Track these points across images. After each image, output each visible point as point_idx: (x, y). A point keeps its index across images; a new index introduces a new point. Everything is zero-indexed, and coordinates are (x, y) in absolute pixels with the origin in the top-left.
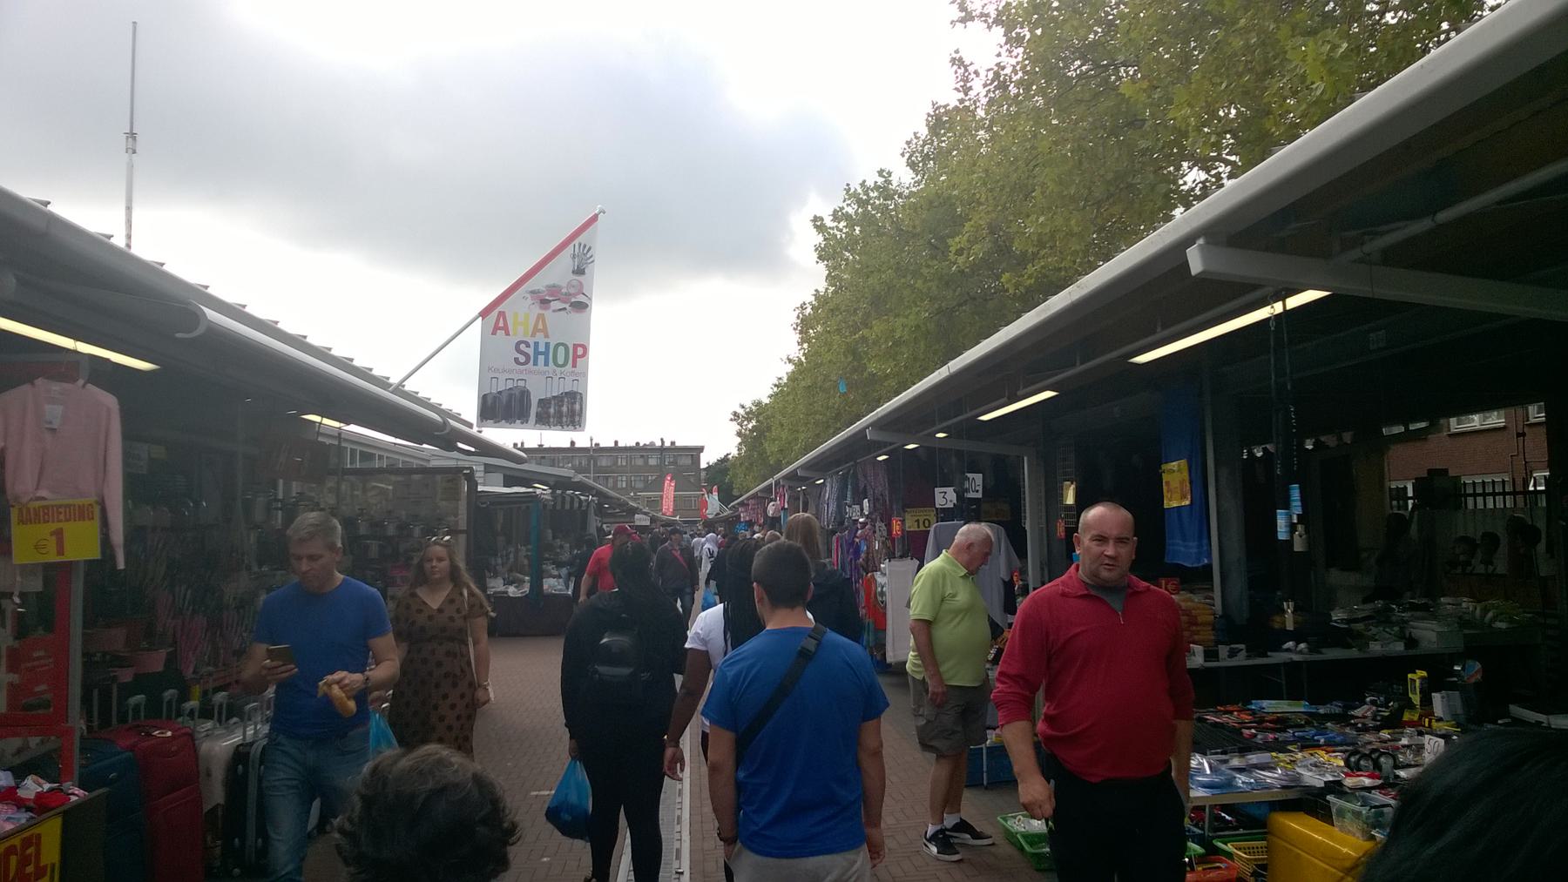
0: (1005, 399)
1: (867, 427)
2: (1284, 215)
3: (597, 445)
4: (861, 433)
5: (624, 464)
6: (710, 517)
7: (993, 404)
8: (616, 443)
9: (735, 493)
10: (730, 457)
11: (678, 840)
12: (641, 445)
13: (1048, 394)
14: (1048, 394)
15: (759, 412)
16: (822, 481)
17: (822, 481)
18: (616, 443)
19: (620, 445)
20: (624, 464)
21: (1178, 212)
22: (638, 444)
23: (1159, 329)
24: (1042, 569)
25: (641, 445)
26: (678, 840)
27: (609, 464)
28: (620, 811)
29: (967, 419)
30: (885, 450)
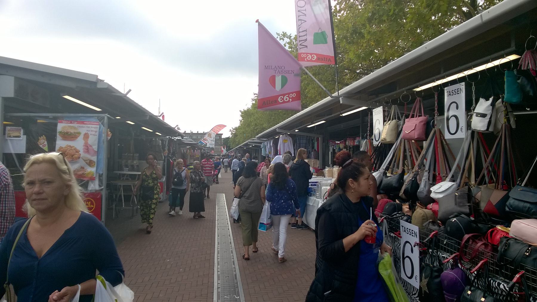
0: (310, 123)
1: (277, 128)
2: (359, 92)
3: (192, 132)
4: (275, 130)
5: (200, 138)
6: (224, 154)
7: (424, 81)
8: (198, 132)
9: (231, 147)
10: (230, 137)
11: (234, 271)
12: (205, 133)
13: (418, 89)
14: (323, 122)
15: (236, 129)
16: (278, 137)
17: (278, 137)
18: (198, 132)
19: (199, 132)
20: (200, 138)
21: (371, 73)
22: (204, 132)
23: (398, 89)
24: (443, 154)
25: (205, 133)
26: (234, 271)
27: (196, 138)
28: (128, 123)
29: (304, 127)
30: (324, 119)
